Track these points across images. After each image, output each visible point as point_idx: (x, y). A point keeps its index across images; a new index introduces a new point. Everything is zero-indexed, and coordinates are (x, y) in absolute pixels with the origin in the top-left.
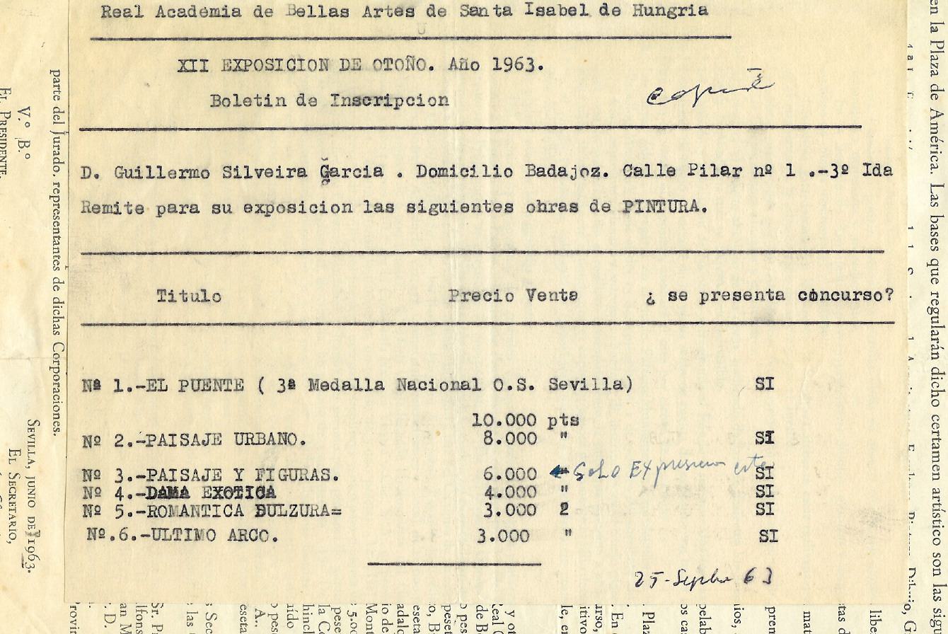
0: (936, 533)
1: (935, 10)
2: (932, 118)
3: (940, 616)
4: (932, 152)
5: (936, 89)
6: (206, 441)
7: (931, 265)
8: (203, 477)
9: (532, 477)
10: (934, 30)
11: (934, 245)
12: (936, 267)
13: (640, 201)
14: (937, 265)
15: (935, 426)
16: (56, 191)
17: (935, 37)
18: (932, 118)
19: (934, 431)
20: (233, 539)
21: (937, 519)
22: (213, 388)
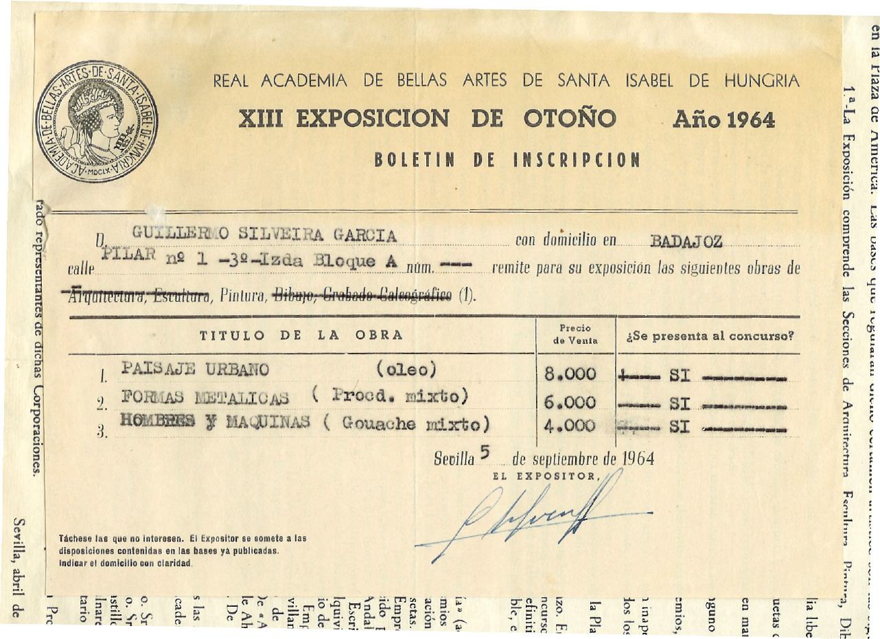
0: (544, 607)
1: (429, 626)
2: (243, 619)
3: (39, 444)
4: (81, 613)
5: (384, 606)
6: (697, 243)
7: (334, 606)
8: (694, 244)
9: (224, 236)
10: (592, 609)
11: (846, 363)
12: (337, 608)
13: (117, 248)
14: (808, 626)
15: (846, 335)
16: (39, 240)
17: (593, 614)
18: (243, 619)
19: (873, 165)
20: (350, 238)
21: (114, 604)
22: (198, 235)
